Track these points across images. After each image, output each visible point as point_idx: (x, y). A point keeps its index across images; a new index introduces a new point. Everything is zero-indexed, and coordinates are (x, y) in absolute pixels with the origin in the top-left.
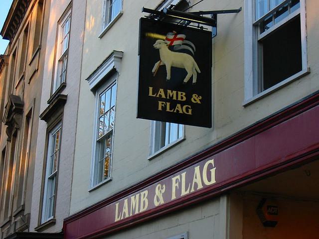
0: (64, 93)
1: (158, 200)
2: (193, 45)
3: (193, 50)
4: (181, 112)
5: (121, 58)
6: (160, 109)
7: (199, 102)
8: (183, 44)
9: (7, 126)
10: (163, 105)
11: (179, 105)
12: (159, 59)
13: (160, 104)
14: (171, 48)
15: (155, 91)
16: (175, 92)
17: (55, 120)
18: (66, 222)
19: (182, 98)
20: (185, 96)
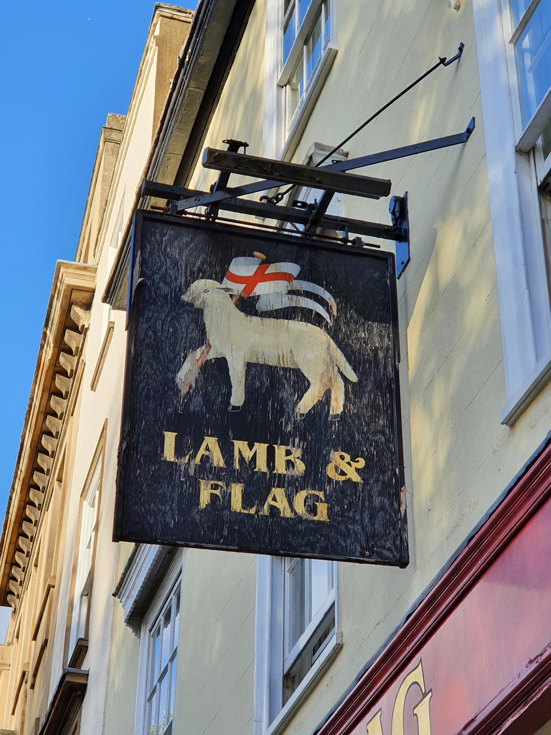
2: (327, 296)
7: (356, 478)
10: (217, 492)
11: (278, 493)
16: (261, 449)
19: (290, 464)
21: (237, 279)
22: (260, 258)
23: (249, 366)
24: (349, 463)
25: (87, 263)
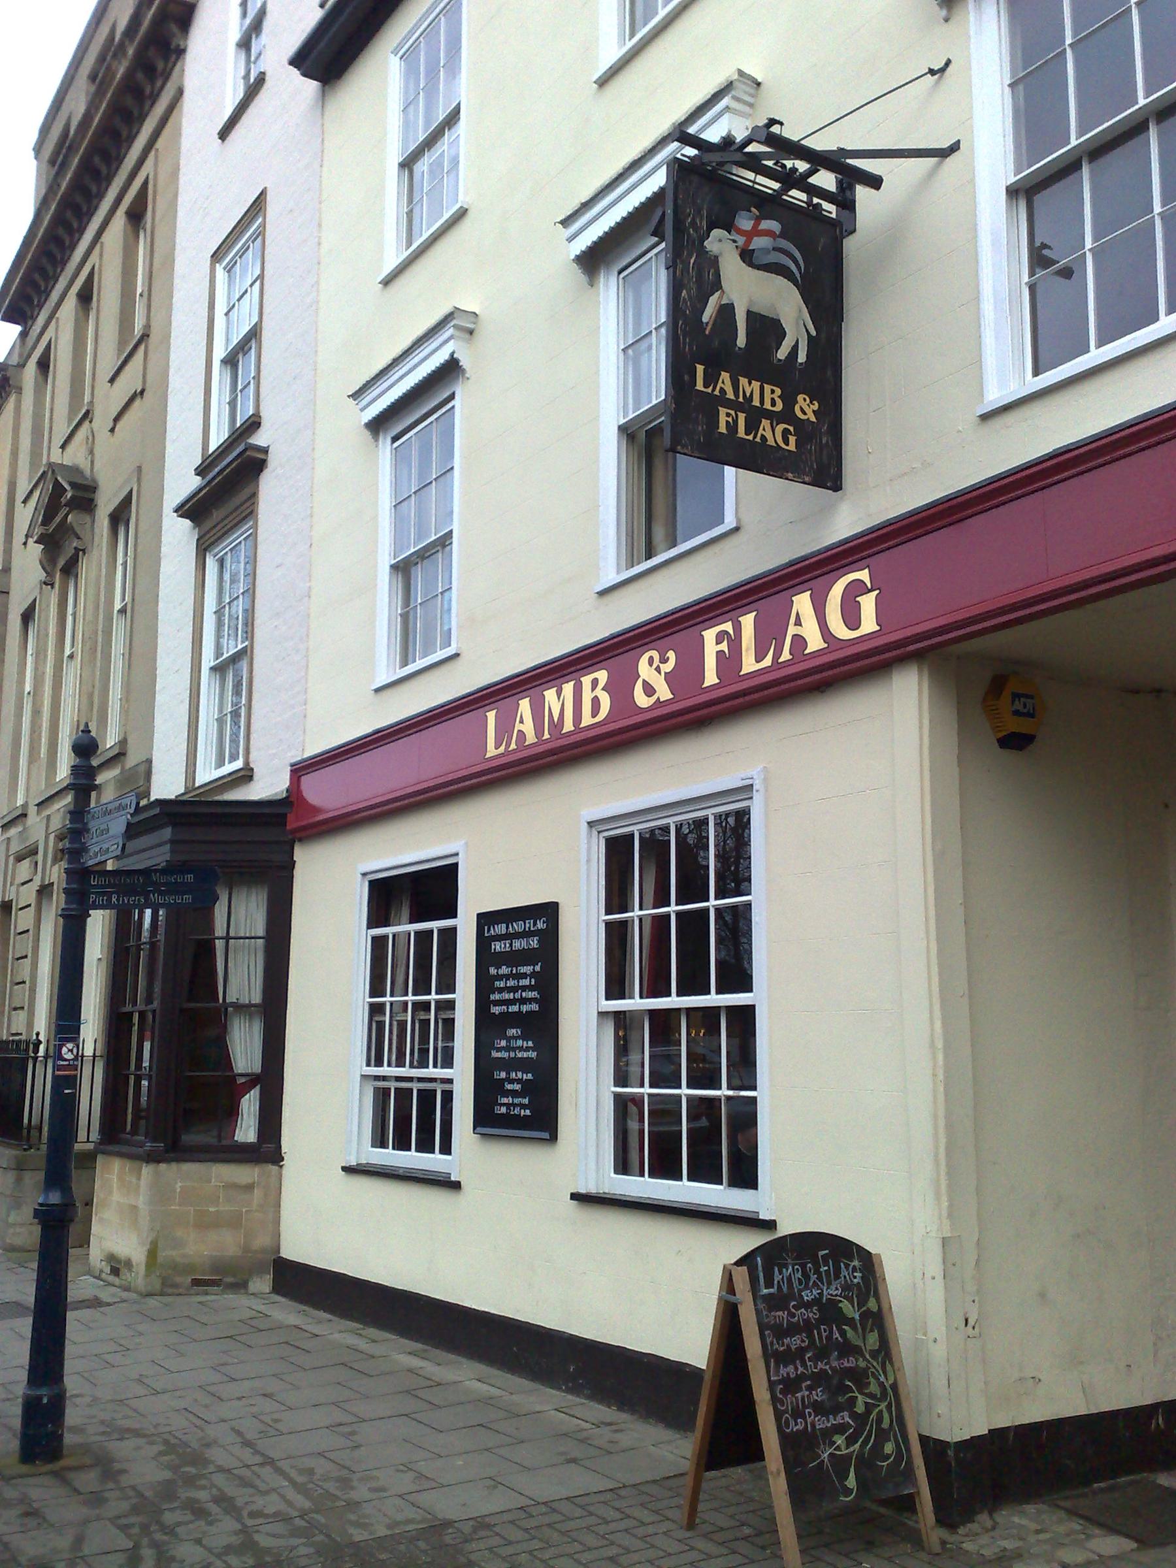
0: (260, 439)
1: (649, 690)
3: (799, 268)
4: (771, 442)
5: (471, 332)
6: (723, 429)
8: (774, 249)
9: (42, 547)
10: (730, 419)
11: (765, 423)
12: (717, 285)
13: (723, 417)
14: (747, 256)
15: (711, 379)
16: (756, 385)
17: (227, 517)
18: (299, 770)
19: (773, 403)
20: (779, 397)
21: (740, 232)
22: (755, 214)
23: (749, 312)
24: (808, 405)
25: (549, 911)
